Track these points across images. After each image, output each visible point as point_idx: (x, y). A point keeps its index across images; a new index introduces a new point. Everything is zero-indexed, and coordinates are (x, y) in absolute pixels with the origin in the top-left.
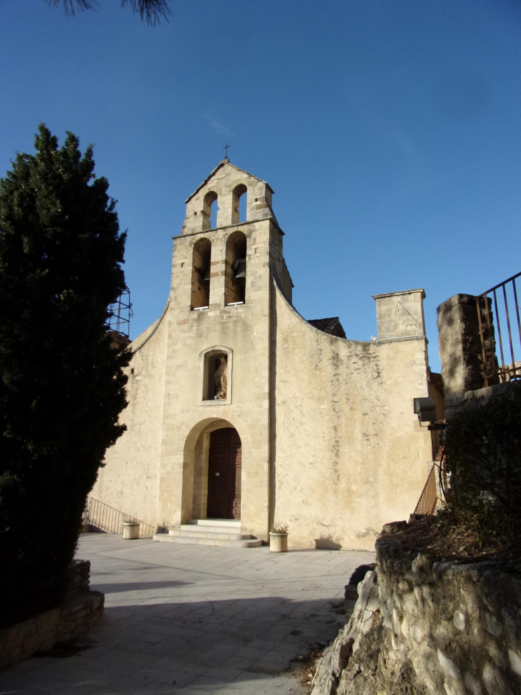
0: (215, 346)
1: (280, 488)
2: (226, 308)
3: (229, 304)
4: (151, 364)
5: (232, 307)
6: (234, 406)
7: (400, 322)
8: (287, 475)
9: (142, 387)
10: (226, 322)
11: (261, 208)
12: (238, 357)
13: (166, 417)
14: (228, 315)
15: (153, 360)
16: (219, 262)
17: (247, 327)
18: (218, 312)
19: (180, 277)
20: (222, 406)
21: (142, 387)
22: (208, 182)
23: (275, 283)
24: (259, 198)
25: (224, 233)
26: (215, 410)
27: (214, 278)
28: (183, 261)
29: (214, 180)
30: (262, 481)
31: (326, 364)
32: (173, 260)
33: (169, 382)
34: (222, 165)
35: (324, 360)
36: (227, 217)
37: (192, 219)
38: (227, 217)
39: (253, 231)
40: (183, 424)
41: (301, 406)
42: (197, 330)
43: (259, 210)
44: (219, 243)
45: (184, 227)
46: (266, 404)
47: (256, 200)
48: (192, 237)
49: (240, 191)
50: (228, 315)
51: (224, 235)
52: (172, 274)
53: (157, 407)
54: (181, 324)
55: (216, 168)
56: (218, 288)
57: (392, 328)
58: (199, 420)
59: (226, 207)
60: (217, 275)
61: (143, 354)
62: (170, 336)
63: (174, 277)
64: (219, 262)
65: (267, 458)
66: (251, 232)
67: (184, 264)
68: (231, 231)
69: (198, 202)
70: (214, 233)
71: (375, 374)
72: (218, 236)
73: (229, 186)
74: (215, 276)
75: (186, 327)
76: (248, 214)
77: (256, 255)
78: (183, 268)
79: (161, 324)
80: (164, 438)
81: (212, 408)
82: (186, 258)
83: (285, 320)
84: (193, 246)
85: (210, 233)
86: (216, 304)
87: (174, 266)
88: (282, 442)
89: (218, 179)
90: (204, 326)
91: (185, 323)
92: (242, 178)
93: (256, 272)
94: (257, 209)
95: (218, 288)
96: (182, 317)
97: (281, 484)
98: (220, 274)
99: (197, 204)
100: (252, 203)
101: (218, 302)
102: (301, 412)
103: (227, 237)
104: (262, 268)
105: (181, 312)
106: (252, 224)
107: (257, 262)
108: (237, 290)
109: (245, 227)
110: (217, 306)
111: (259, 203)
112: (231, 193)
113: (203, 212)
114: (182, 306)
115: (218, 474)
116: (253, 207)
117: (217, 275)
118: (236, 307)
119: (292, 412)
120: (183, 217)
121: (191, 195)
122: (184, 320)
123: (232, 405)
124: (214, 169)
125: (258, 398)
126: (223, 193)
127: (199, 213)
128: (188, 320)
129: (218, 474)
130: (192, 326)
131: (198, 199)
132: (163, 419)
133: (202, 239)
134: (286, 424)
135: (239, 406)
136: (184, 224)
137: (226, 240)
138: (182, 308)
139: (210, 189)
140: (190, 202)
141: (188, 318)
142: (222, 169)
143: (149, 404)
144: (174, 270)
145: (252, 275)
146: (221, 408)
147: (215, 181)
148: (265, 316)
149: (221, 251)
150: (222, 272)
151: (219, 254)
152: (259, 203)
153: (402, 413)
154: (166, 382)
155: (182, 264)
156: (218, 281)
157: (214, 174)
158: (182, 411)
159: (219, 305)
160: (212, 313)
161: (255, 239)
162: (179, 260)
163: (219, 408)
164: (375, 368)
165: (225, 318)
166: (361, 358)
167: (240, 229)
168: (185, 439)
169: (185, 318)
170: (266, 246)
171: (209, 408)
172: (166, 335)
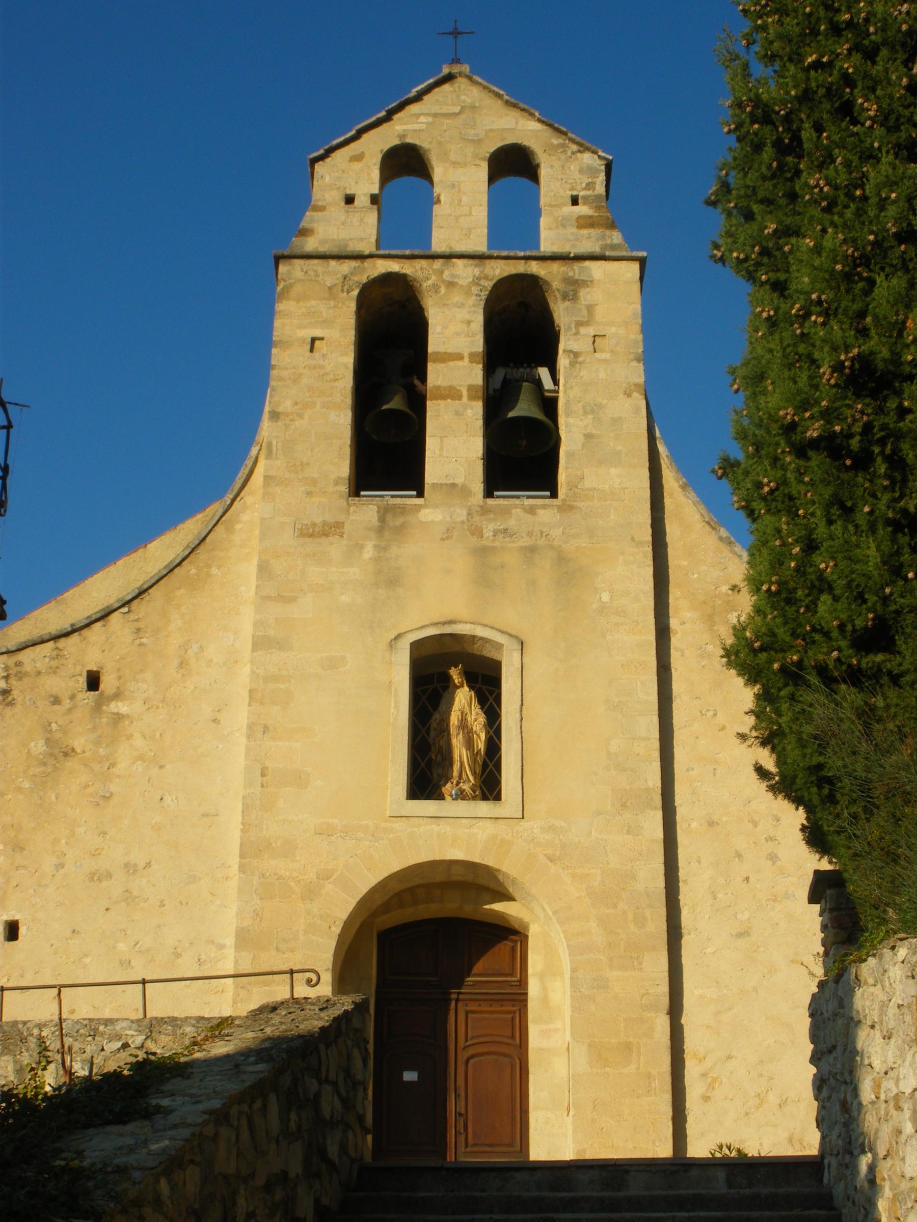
0: (451, 622)
1: (706, 1098)
2: (490, 501)
3: (496, 493)
4: (176, 662)
5: (517, 501)
6: (532, 826)
8: (729, 1057)
9: (138, 741)
10: (493, 549)
11: (592, 226)
12: (539, 665)
13: (251, 851)
14: (499, 525)
15: (185, 647)
16: (460, 357)
17: (569, 573)
18: (461, 514)
19: (304, 381)
20: (488, 823)
21: (138, 741)
22: (396, 117)
23: (662, 449)
24: (585, 198)
25: (477, 271)
26: (452, 831)
27: (442, 403)
28: (318, 333)
29: (418, 116)
30: (649, 1075)
32: (277, 323)
33: (266, 729)
34: (449, 78)
36: (470, 230)
37: (338, 211)
38: (470, 230)
39: (584, 283)
40: (325, 876)
41: (770, 839)
42: (377, 560)
43: (585, 232)
44: (457, 298)
45: (305, 233)
46: (652, 824)
47: (575, 201)
48: (354, 264)
49: (512, 165)
50: (499, 525)
51: (476, 281)
52: (274, 367)
53: (206, 815)
54: (311, 536)
55: (431, 81)
56: (454, 441)
58: (396, 865)
59: (465, 199)
60: (452, 394)
61: (141, 625)
62: (263, 569)
63: (281, 379)
64: (460, 357)
65: (665, 1001)
66: (573, 288)
67: (317, 343)
68: (499, 270)
69: (356, 166)
70: (438, 264)
72: (453, 276)
73: (478, 142)
74: (444, 397)
75: (335, 548)
76: (544, 234)
77: (597, 355)
78: (316, 354)
79: (220, 529)
80: (245, 924)
81: (445, 828)
82: (327, 323)
83: (703, 568)
84: (356, 292)
85: (424, 263)
86: (453, 485)
87: (285, 344)
88: (709, 950)
89: (435, 115)
90: (406, 552)
91: (326, 535)
92: (526, 130)
93: (600, 407)
94: (580, 227)
95: (454, 441)
96: (316, 515)
97: (711, 1086)
98: (465, 393)
99: (352, 172)
100: (560, 206)
101: (459, 481)
102: (773, 858)
103: (489, 285)
104: (621, 396)
105: (309, 493)
106: (577, 266)
107: (602, 375)
108: (522, 457)
109: (555, 267)
110: (452, 489)
111: (583, 209)
112: (485, 165)
113: (374, 199)
114: (316, 475)
115: (410, 1076)
116: (564, 218)
117: (452, 394)
118: (522, 510)
119: (739, 855)
120: (301, 199)
121: (335, 142)
122: (325, 523)
123: (523, 823)
124: (422, 83)
125: (624, 805)
126: (453, 157)
127: (362, 200)
128: (339, 525)
129: (410, 1076)
130: (875, 308)
131: (358, 158)
132: (242, 856)
133: (388, 279)
134: (720, 896)
135: (552, 828)
136: (304, 224)
137: (484, 295)
138: (314, 482)
139: (402, 136)
140: (328, 160)
141: (341, 518)
142: (446, 87)
143: (168, 799)
144: (278, 356)
145: (585, 413)
146: (483, 832)
148: (640, 544)
149: (469, 322)
150: (470, 388)
151: (455, 331)
152: (583, 209)
154: (251, 727)
155: (313, 340)
156: (457, 413)
157: (418, 98)
158: (325, 832)
159: (464, 491)
160: (430, 513)
161: (590, 308)
162: (300, 327)
163: (474, 830)
165: (488, 533)
167: (534, 268)
168: (337, 930)
169: (330, 518)
170: (632, 337)
171: (434, 827)
172: (251, 568)
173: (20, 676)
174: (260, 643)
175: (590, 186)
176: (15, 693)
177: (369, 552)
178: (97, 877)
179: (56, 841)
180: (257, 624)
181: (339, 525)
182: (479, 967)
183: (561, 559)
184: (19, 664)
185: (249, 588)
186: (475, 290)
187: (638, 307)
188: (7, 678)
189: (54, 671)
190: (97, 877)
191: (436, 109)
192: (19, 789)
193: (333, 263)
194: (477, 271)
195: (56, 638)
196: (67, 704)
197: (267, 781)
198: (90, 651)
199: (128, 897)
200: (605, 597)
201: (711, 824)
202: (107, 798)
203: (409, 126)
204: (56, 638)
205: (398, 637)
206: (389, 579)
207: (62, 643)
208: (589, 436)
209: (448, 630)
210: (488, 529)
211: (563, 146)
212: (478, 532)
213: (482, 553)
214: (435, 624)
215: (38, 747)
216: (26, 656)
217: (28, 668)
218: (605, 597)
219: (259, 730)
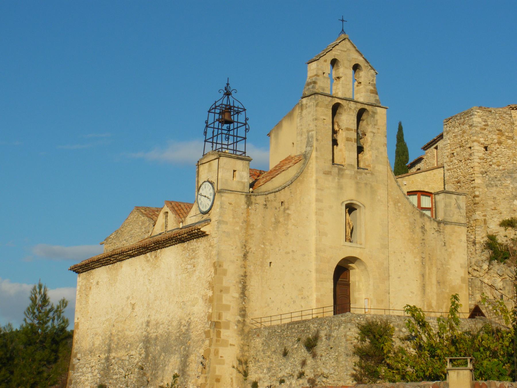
0: (352, 200)
7: (456, 213)
9: (293, 221)
13: (318, 251)
18: (353, 173)
31: (418, 230)
35: (417, 228)
51: (356, 108)
54: (325, 174)
57: (451, 215)
64: (352, 130)
71: (443, 244)
89: (341, 51)
94: (371, 93)
102: (404, 261)
103: (358, 110)
147: (339, 51)
150: (355, 139)
153: (456, 271)
164: (443, 240)
165: (358, 179)
166: (436, 231)
173: (269, 201)
174: (317, 200)
175: (373, 80)
176: (268, 205)
177: (336, 180)
178: (287, 253)
179: (278, 244)
180: (317, 195)
181: (331, 172)
182: (341, 276)
183: (372, 187)
184: (268, 198)
185: (314, 185)
186: (355, 111)
187: (386, 122)
188: (266, 201)
189: (275, 200)
190: (287, 253)
191: (341, 49)
192: (270, 230)
193: (327, 97)
194: (355, 106)
195: (275, 192)
196: (278, 209)
197: (321, 234)
198: (283, 196)
199: (294, 259)
200: (379, 198)
201: (394, 252)
202: (288, 234)
203: (335, 53)
204: (275, 192)
205: (343, 202)
206: (340, 187)
207: (276, 194)
208: (376, 156)
209: (352, 202)
210: (358, 177)
211: (367, 66)
212: (356, 178)
213: (357, 183)
214: (349, 200)
215: (273, 220)
216: (269, 196)
217: (269, 199)
218: (379, 198)
219: (318, 222)
